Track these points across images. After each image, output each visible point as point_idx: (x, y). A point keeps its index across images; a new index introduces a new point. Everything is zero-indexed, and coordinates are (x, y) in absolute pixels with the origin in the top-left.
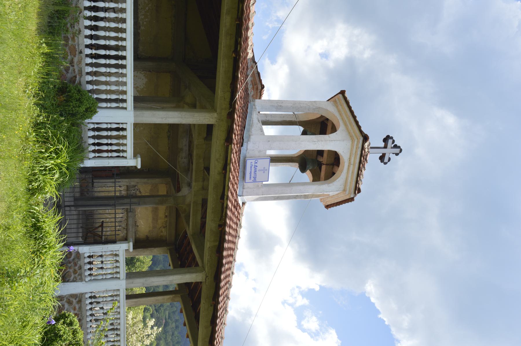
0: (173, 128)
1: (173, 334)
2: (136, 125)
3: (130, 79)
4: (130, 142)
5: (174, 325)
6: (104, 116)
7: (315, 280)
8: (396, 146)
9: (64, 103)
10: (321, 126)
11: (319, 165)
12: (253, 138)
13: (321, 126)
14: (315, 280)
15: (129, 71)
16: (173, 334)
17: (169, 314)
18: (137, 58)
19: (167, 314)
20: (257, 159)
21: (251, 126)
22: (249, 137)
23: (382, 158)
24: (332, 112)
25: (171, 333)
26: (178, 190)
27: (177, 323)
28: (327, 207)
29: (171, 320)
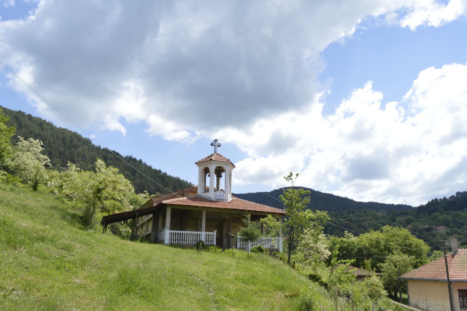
0: (207, 220)
1: (358, 216)
2: (206, 231)
3: (188, 232)
4: (210, 233)
5: (351, 215)
6: (203, 239)
7: (317, 107)
8: (215, 141)
9: (200, 246)
10: (206, 171)
11: (219, 172)
12: (210, 196)
13: (206, 171)
14: (317, 107)
15: (186, 232)
16: (358, 216)
17: (343, 218)
18: (182, 230)
19: (343, 220)
20: (216, 195)
21: (206, 197)
22: (210, 198)
23: (219, 146)
24: (203, 167)
25: (357, 217)
26: (226, 219)
27: (350, 212)
28: (235, 167)
29: (347, 217)
